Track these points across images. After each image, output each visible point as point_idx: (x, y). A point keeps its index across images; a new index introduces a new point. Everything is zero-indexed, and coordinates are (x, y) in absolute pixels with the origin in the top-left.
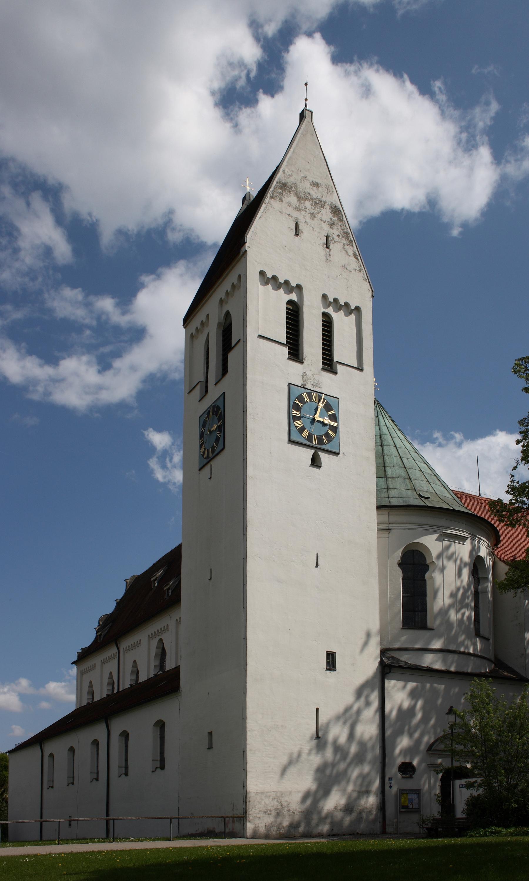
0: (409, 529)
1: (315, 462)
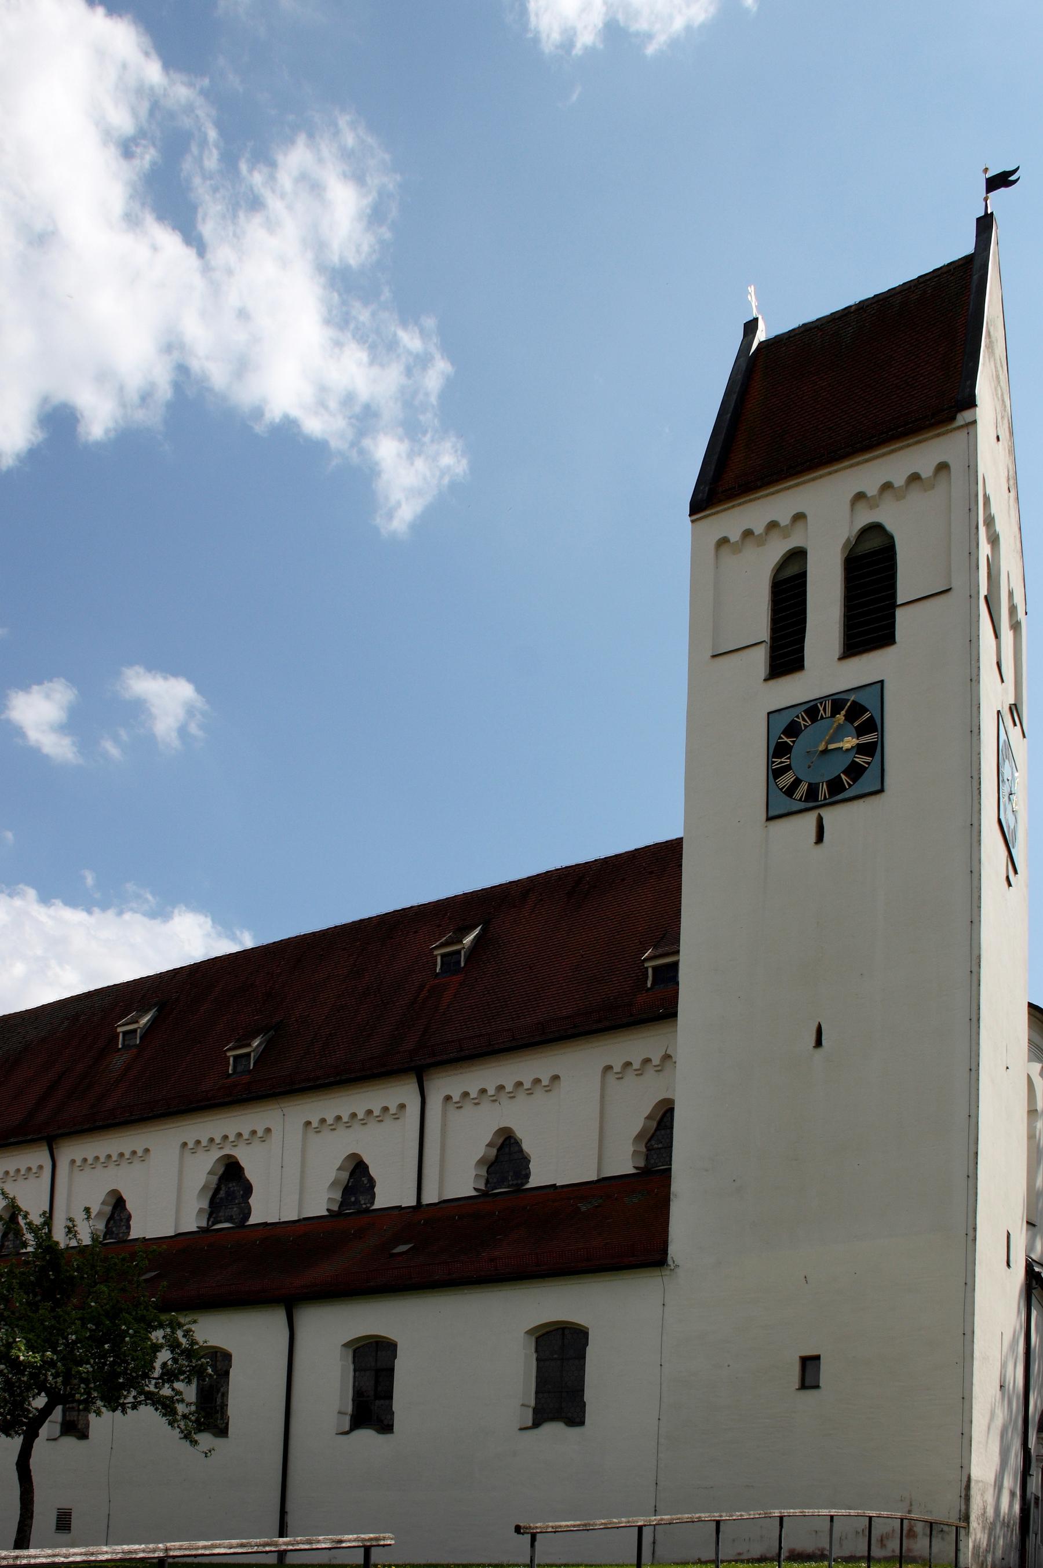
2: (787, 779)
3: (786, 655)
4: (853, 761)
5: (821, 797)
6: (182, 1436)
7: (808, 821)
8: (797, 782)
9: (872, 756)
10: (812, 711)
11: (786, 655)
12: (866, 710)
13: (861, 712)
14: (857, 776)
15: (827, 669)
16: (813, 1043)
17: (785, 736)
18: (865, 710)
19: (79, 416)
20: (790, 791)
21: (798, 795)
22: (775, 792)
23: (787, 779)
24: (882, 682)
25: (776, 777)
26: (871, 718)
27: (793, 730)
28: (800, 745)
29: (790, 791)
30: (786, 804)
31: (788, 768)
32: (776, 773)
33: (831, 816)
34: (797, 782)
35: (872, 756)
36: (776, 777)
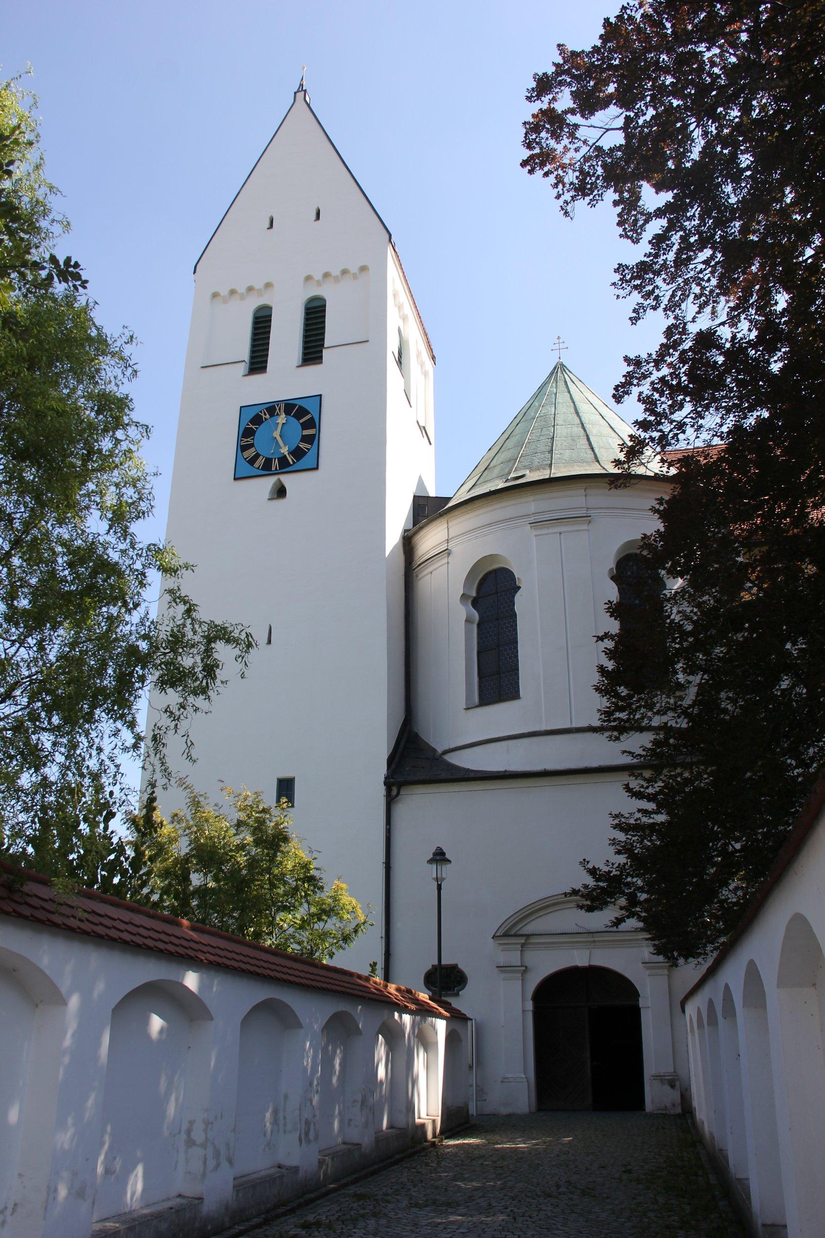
0: (476, 516)
1: (280, 492)
2: (250, 453)
3: (258, 362)
4: (298, 447)
5: (273, 469)
6: (526, 154)
7: (269, 482)
8: (257, 456)
9: (311, 444)
10: (272, 409)
11: (258, 362)
12: (308, 413)
13: (304, 414)
14: (303, 454)
15: (285, 378)
16: (266, 641)
17: (253, 422)
18: (308, 413)
19: (178, 1211)
20: (252, 461)
21: (256, 465)
22: (242, 462)
23: (250, 453)
24: (321, 395)
25: (242, 451)
26: (312, 419)
27: (257, 420)
28: (261, 431)
29: (252, 461)
30: (247, 469)
31: (252, 446)
32: (243, 448)
33: (288, 480)
34: (257, 456)
35: (311, 444)
36: (242, 451)
